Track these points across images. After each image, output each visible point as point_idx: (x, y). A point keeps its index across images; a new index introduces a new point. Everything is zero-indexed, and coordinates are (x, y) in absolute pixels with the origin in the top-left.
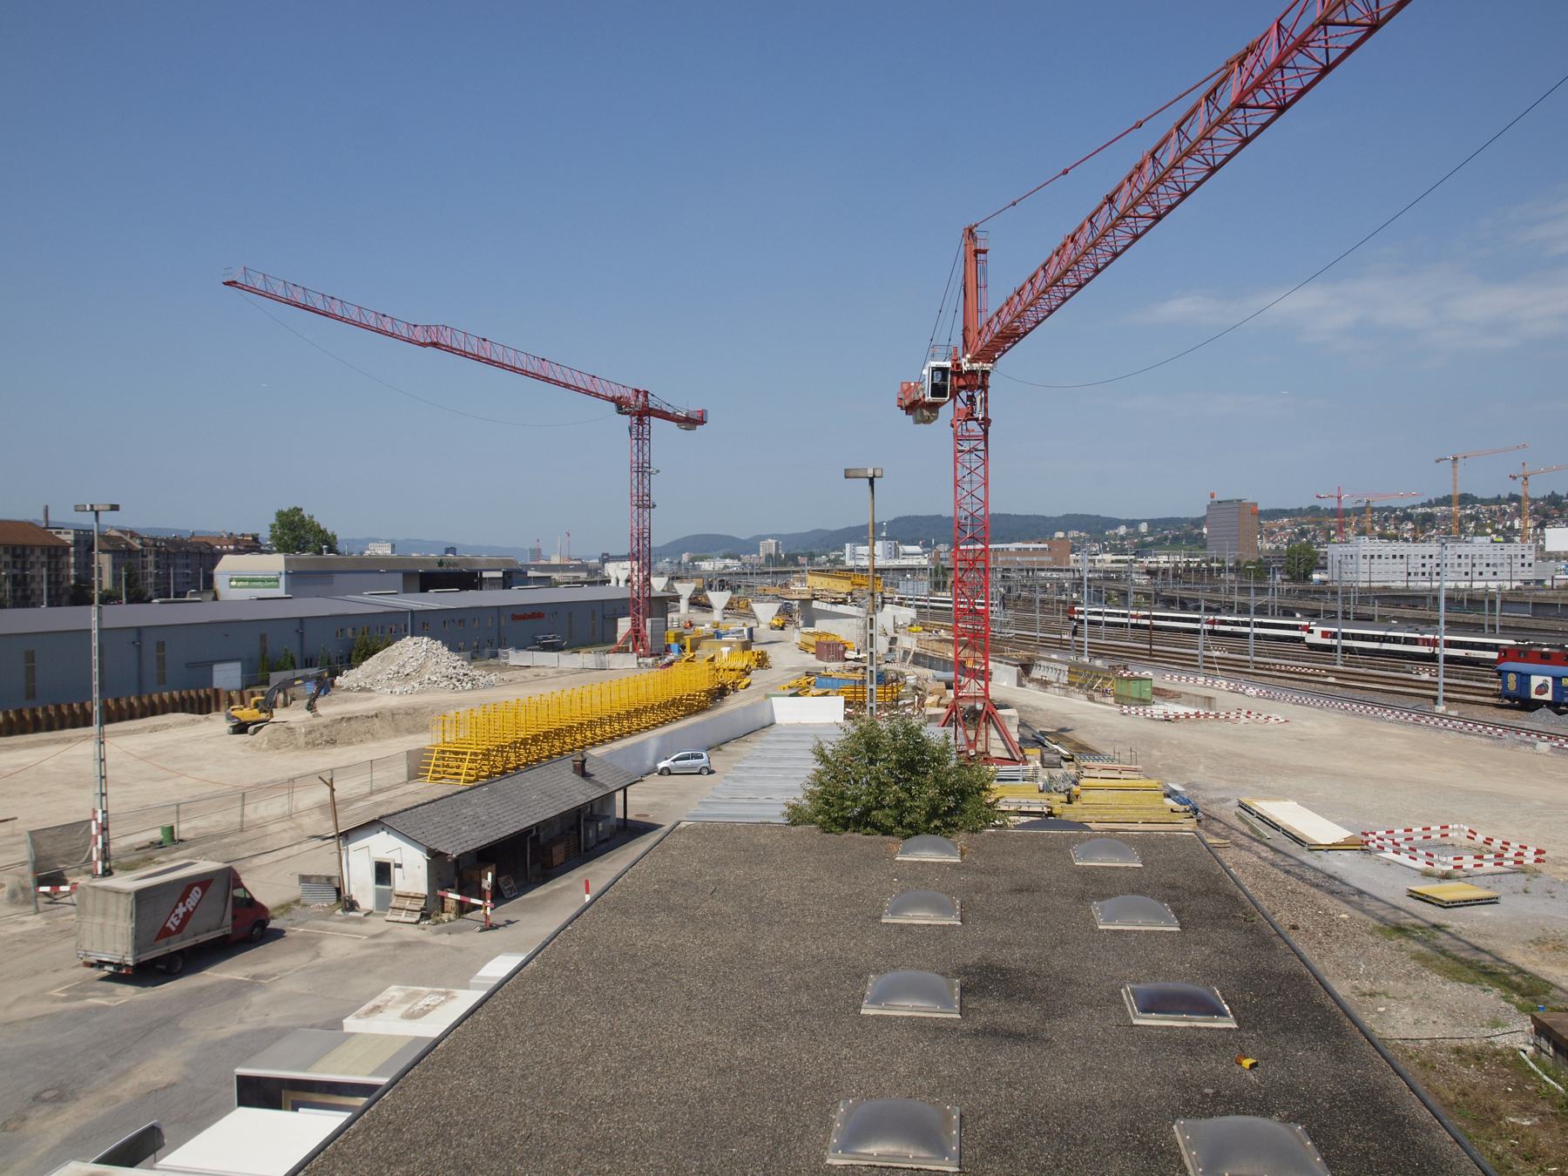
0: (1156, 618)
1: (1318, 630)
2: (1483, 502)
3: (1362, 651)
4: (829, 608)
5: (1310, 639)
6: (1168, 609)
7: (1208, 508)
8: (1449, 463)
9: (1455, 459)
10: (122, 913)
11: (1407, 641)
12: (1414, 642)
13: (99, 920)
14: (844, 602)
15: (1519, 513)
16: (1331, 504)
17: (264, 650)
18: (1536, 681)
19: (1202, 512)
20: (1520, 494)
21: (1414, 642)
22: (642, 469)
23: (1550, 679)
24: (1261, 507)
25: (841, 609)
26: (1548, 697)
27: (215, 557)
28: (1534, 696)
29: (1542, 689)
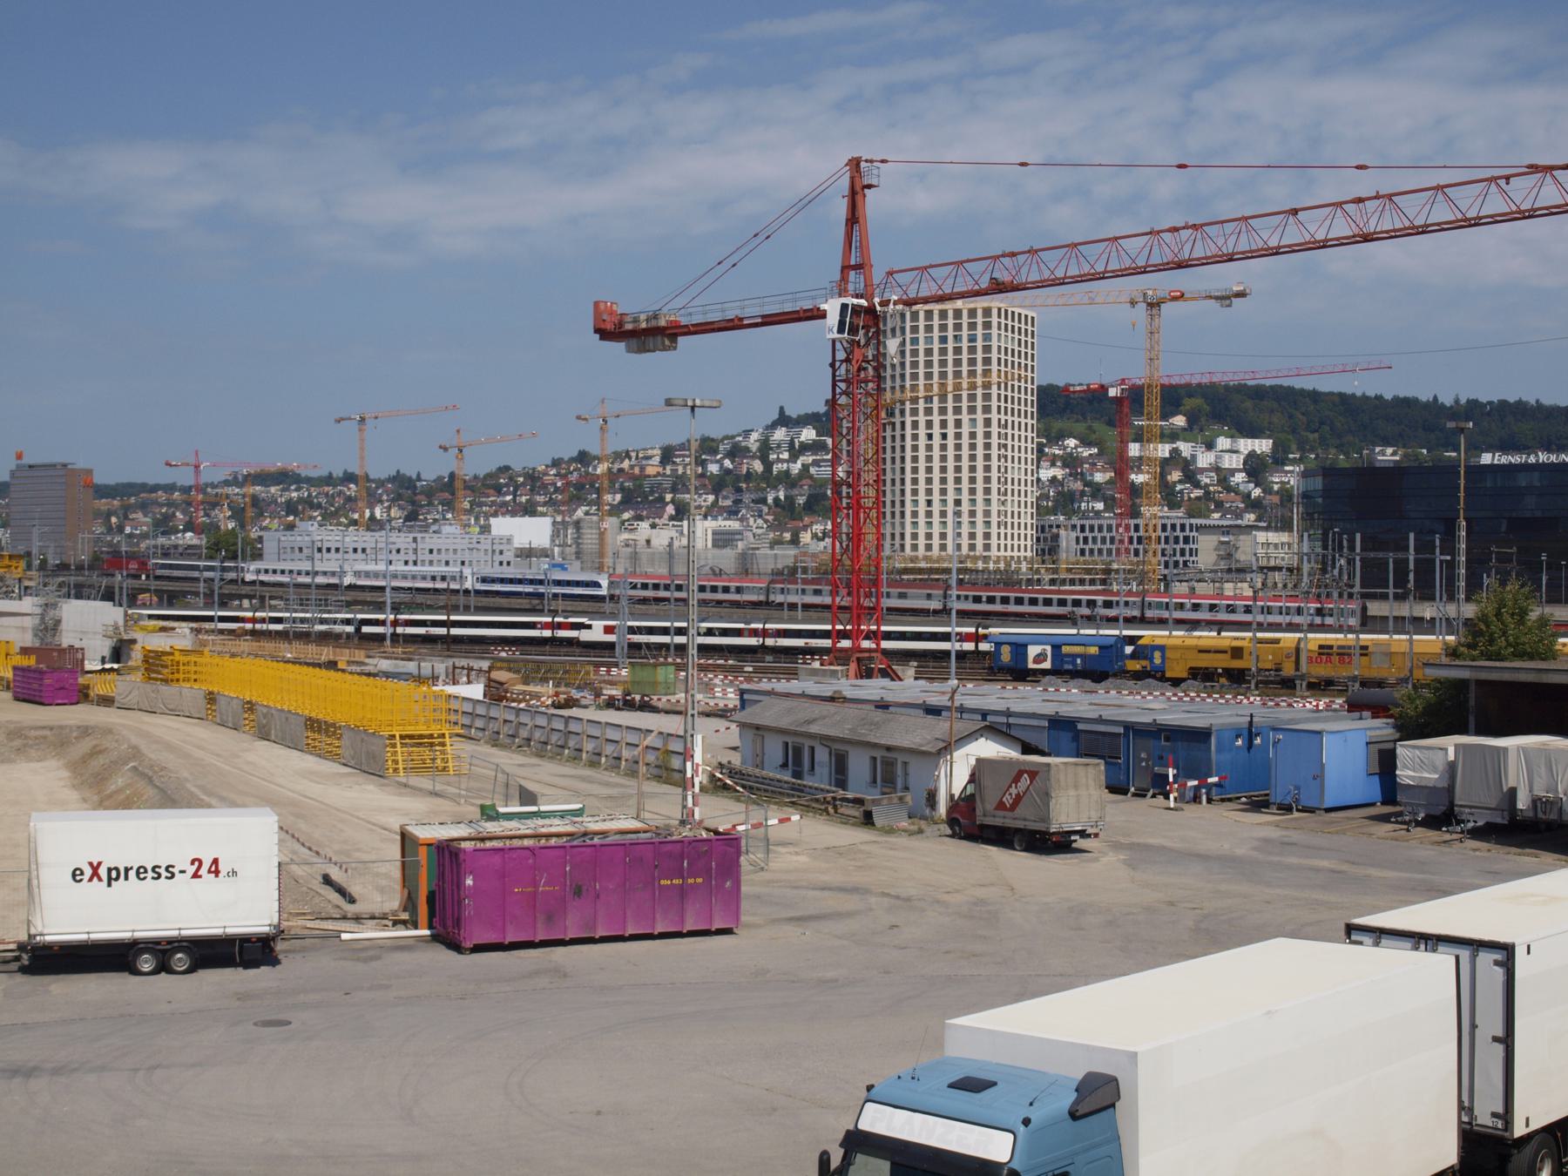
0: (560, 626)
1: (599, 625)
2: (310, 481)
3: (231, 632)
5: (585, 635)
6: (171, 605)
7: (13, 473)
8: (354, 425)
9: (363, 420)
10: (1091, 783)
11: (725, 633)
12: (738, 633)
13: (1072, 792)
15: (373, 500)
16: (185, 478)
18: (1033, 651)
21: (738, 633)
22: (362, 458)
23: (1049, 648)
24: (98, 479)
27: (1026, 646)
29: (1040, 658)
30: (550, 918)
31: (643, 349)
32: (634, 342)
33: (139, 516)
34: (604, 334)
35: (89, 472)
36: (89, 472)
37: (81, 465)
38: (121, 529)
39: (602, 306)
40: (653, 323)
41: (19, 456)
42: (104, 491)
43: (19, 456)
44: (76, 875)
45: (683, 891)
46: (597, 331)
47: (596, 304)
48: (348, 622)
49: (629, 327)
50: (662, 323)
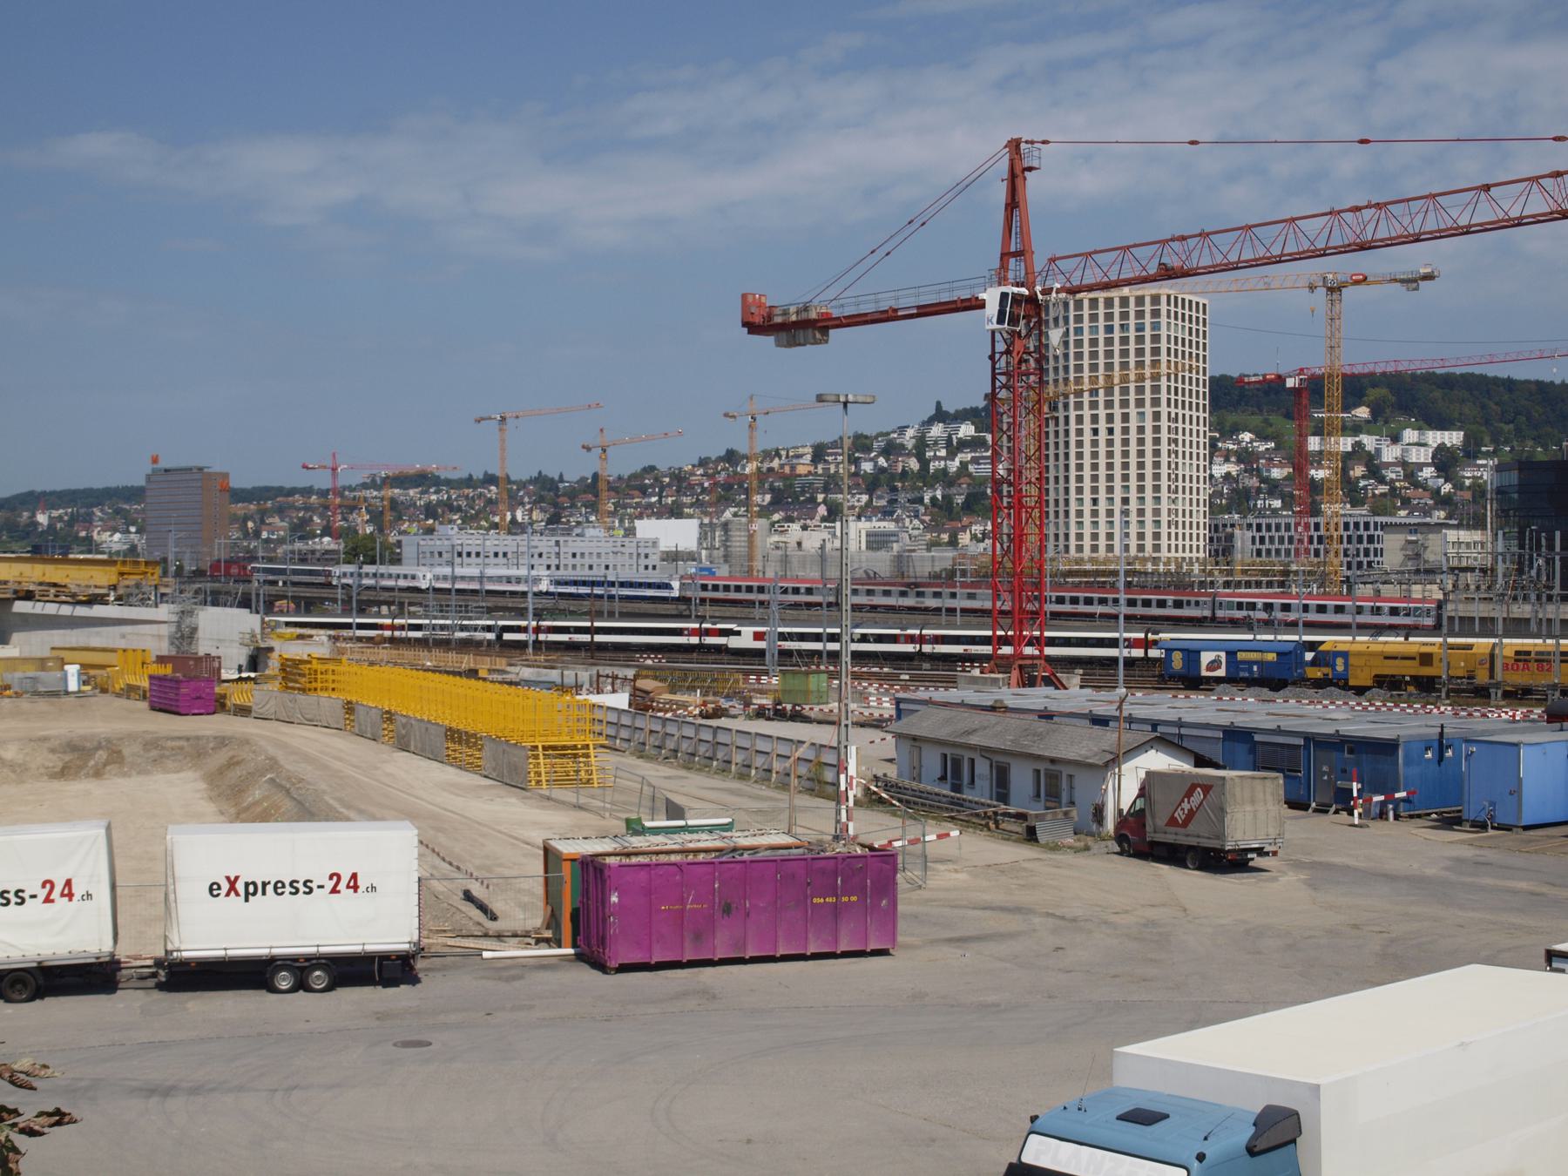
1: (748, 631)
2: (449, 483)
4: (66, 610)
5: (733, 643)
7: (148, 477)
8: (494, 425)
9: (503, 419)
10: (1269, 797)
11: (880, 639)
12: (894, 639)
13: (1248, 808)
14: (93, 600)
16: (322, 481)
17: (1441, 734)
18: (1206, 657)
19: (140, 481)
20: (498, 473)
21: (894, 639)
23: (1223, 655)
24: (235, 483)
25: (98, 611)
26: (1221, 673)
28: (1204, 673)
29: (1214, 665)
30: (698, 936)
31: (793, 343)
32: (783, 335)
33: (276, 520)
34: (752, 328)
35: (226, 476)
36: (226, 476)
37: (217, 469)
38: (257, 534)
39: (750, 299)
40: (804, 316)
41: (155, 460)
42: (240, 496)
43: (155, 460)
44: (213, 889)
45: (836, 911)
46: (745, 324)
47: (744, 297)
48: (489, 629)
49: (778, 320)
50: (813, 315)
